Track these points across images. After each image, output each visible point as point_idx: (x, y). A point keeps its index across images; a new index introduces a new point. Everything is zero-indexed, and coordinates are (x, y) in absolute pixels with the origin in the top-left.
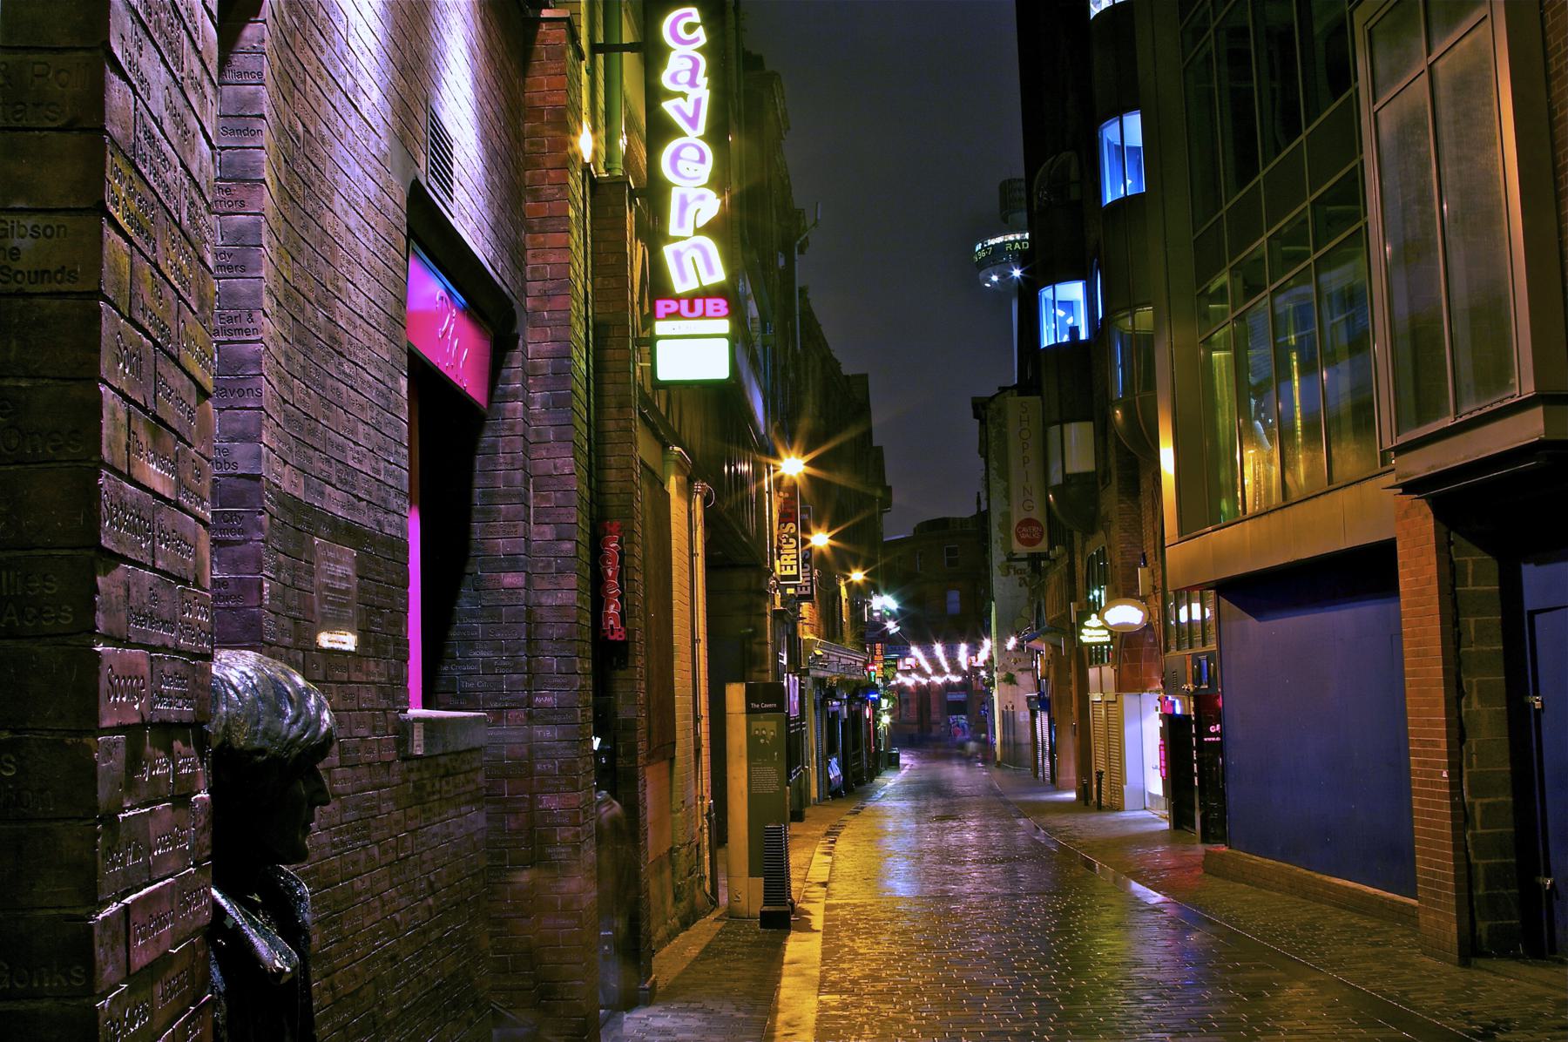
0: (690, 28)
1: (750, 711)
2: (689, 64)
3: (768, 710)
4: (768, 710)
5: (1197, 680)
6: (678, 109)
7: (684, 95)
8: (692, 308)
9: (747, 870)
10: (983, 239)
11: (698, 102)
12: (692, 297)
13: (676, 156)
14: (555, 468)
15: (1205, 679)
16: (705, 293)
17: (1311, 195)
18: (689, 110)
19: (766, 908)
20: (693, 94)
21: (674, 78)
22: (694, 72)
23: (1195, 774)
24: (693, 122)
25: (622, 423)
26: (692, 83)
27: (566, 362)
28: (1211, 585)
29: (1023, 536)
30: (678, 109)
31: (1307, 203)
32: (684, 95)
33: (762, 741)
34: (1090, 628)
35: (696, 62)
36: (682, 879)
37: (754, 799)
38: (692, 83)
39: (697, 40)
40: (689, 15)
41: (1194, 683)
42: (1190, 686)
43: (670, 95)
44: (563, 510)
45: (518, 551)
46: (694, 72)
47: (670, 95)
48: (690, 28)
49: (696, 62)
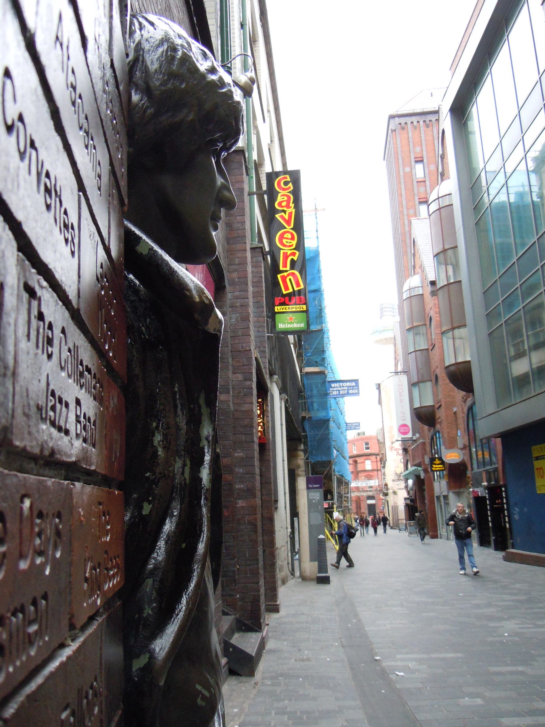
0: (286, 183)
1: (308, 488)
2: (286, 198)
3: (316, 488)
4: (316, 488)
5: (489, 481)
6: (282, 217)
7: (284, 212)
9: (309, 559)
11: (290, 214)
13: (282, 237)
14: (242, 348)
15: (493, 479)
17: (541, 263)
18: (286, 217)
20: (288, 211)
21: (280, 204)
22: (288, 202)
24: (288, 223)
25: (262, 349)
27: (246, 300)
28: (498, 435)
29: (402, 431)
30: (282, 217)
31: (539, 267)
32: (284, 212)
33: (314, 501)
34: (436, 464)
35: (289, 198)
36: (282, 561)
37: (310, 526)
38: (288, 206)
39: (290, 188)
41: (487, 482)
42: (485, 484)
43: (278, 211)
44: (246, 367)
47: (278, 211)
48: (286, 183)
49: (289, 198)
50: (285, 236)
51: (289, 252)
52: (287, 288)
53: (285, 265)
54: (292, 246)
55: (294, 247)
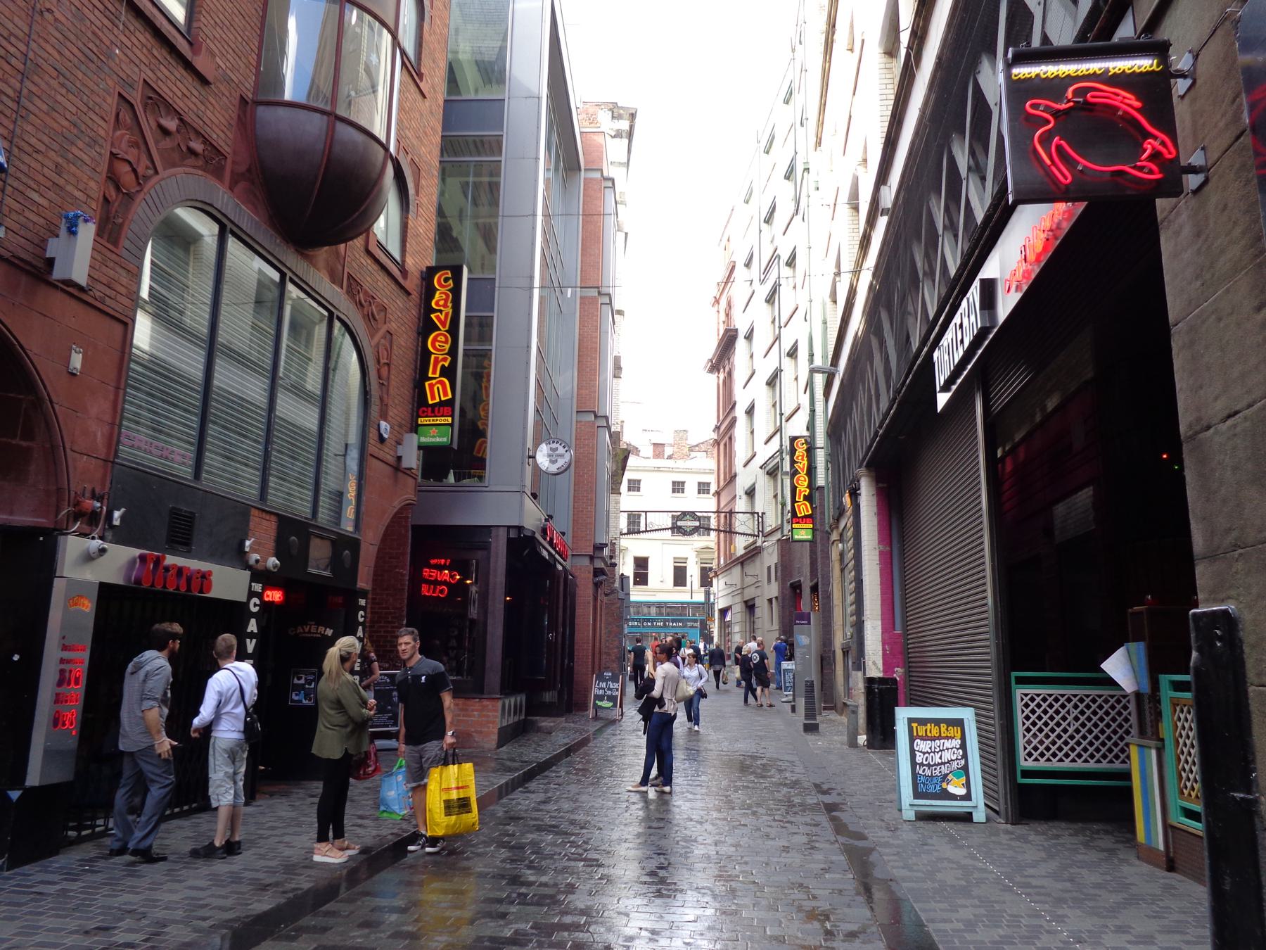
0: (446, 280)
6: (438, 317)
7: (441, 311)
8: (433, 411)
10: (1131, 608)
12: (802, 517)
16: (806, 516)
19: (806, 722)
20: (803, 462)
23: (190, 807)
24: (444, 324)
26: (445, 306)
30: (438, 317)
32: (441, 311)
38: (803, 460)
40: (447, 274)
45: (256, 519)
46: (803, 456)
48: (446, 280)
50: (439, 339)
51: (441, 357)
52: (433, 398)
53: (434, 372)
54: (444, 350)
55: (446, 351)
